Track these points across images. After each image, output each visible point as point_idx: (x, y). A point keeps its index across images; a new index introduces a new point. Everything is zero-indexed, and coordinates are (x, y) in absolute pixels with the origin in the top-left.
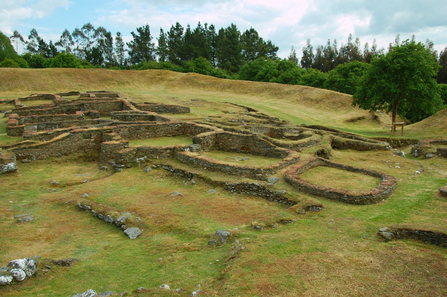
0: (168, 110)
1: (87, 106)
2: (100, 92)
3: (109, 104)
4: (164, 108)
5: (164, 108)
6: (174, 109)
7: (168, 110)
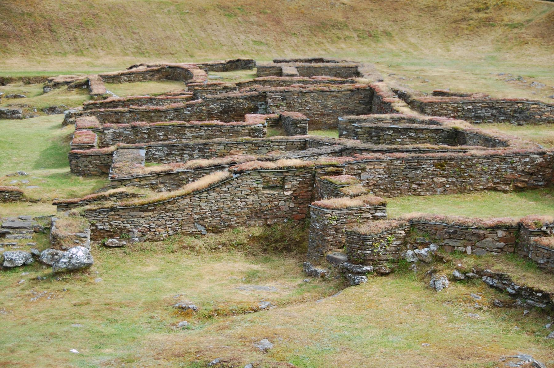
0: (504, 114)
1: (274, 99)
2: (310, 61)
3: (334, 94)
4: (492, 108)
5: (492, 108)
6: (522, 111)
7: (504, 114)
